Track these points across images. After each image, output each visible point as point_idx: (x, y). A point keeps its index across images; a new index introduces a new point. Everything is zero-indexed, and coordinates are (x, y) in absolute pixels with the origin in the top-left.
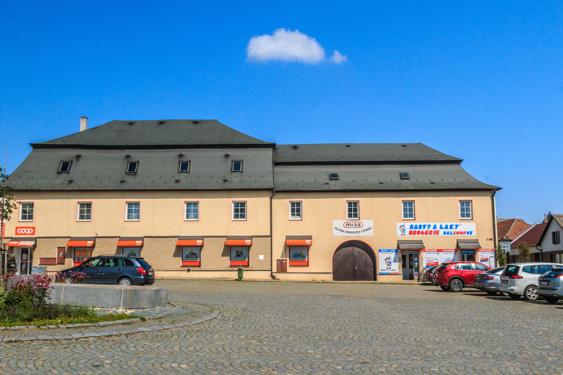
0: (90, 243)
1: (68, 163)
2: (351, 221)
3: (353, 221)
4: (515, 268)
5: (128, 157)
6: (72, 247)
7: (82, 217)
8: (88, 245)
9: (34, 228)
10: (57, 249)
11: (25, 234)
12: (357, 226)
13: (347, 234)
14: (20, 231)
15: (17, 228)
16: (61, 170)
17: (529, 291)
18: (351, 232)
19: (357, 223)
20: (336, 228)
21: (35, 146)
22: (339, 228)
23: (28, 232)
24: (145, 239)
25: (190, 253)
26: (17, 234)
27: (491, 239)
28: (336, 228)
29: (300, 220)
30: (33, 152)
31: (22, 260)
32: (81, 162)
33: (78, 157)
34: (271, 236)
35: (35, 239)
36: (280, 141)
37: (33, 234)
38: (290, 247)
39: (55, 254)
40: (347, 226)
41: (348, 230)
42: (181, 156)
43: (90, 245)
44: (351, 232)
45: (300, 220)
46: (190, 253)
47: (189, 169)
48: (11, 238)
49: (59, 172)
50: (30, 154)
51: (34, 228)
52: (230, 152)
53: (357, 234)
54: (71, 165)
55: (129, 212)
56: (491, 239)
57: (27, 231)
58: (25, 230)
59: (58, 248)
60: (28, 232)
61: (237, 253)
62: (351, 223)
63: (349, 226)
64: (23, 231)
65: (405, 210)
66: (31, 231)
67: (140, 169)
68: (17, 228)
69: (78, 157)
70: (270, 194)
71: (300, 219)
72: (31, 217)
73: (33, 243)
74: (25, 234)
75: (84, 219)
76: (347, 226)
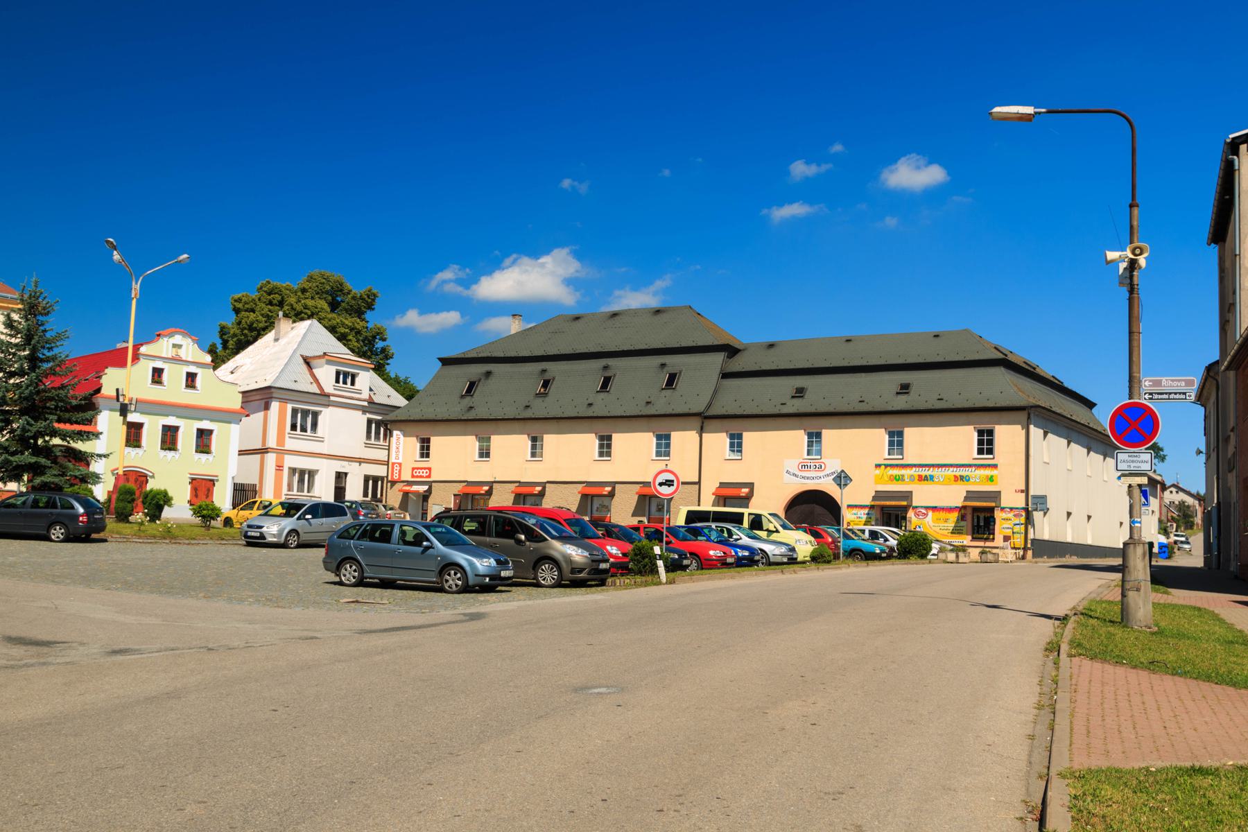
0: (745, 490)
1: (675, 374)
2: (810, 461)
3: (812, 461)
4: (654, 529)
5: (663, 365)
6: (468, 494)
7: (601, 454)
8: (741, 495)
9: (430, 469)
10: (453, 497)
11: (421, 477)
12: (817, 469)
13: (803, 480)
14: (416, 472)
15: (413, 469)
16: (601, 388)
17: (58, 537)
18: (808, 478)
19: (817, 465)
20: (787, 472)
21: (446, 362)
22: (792, 471)
23: (398, 468)
24: (547, 485)
25: (600, 505)
26: (413, 476)
27: (1022, 491)
28: (787, 472)
29: (900, 459)
30: (441, 368)
31: (423, 510)
32: (492, 381)
33: (488, 374)
34: (699, 483)
35: (430, 484)
36: (741, 335)
37: (429, 476)
38: (725, 499)
39: (451, 503)
40: (803, 469)
41: (804, 474)
42: (606, 368)
43: (744, 495)
44: (808, 478)
45: (900, 459)
46: (600, 505)
47: (610, 387)
48: (407, 482)
49: (462, 396)
50: (438, 372)
51: (430, 469)
52: (667, 359)
53: (816, 481)
54: (477, 386)
55: (808, 446)
56: (1022, 491)
57: (423, 472)
58: (395, 471)
59: (455, 495)
60: (425, 475)
61: (658, 506)
62: (809, 464)
63: (806, 469)
64: (419, 472)
65: (980, 442)
66: (427, 472)
67: (681, 384)
68: (413, 469)
69: (488, 374)
70: (696, 422)
71: (740, 458)
72: (990, 451)
73: (426, 488)
74: (421, 477)
75: (661, 456)
76: (803, 469)
